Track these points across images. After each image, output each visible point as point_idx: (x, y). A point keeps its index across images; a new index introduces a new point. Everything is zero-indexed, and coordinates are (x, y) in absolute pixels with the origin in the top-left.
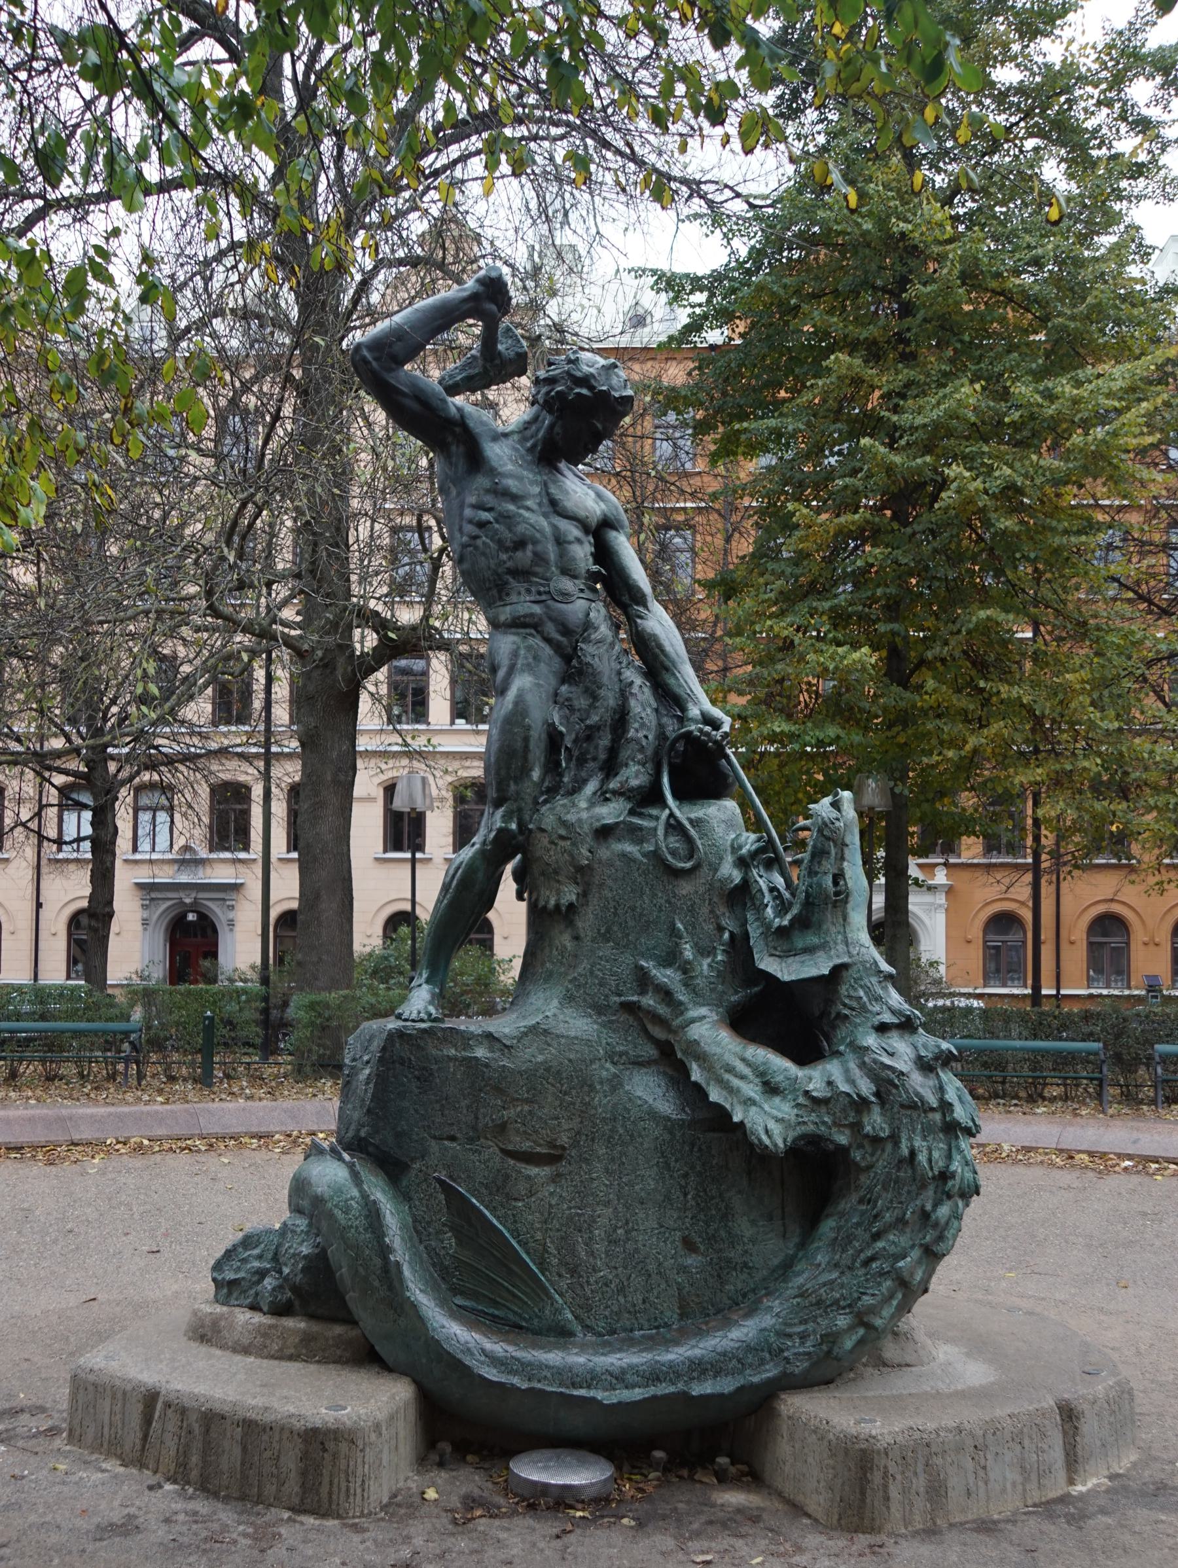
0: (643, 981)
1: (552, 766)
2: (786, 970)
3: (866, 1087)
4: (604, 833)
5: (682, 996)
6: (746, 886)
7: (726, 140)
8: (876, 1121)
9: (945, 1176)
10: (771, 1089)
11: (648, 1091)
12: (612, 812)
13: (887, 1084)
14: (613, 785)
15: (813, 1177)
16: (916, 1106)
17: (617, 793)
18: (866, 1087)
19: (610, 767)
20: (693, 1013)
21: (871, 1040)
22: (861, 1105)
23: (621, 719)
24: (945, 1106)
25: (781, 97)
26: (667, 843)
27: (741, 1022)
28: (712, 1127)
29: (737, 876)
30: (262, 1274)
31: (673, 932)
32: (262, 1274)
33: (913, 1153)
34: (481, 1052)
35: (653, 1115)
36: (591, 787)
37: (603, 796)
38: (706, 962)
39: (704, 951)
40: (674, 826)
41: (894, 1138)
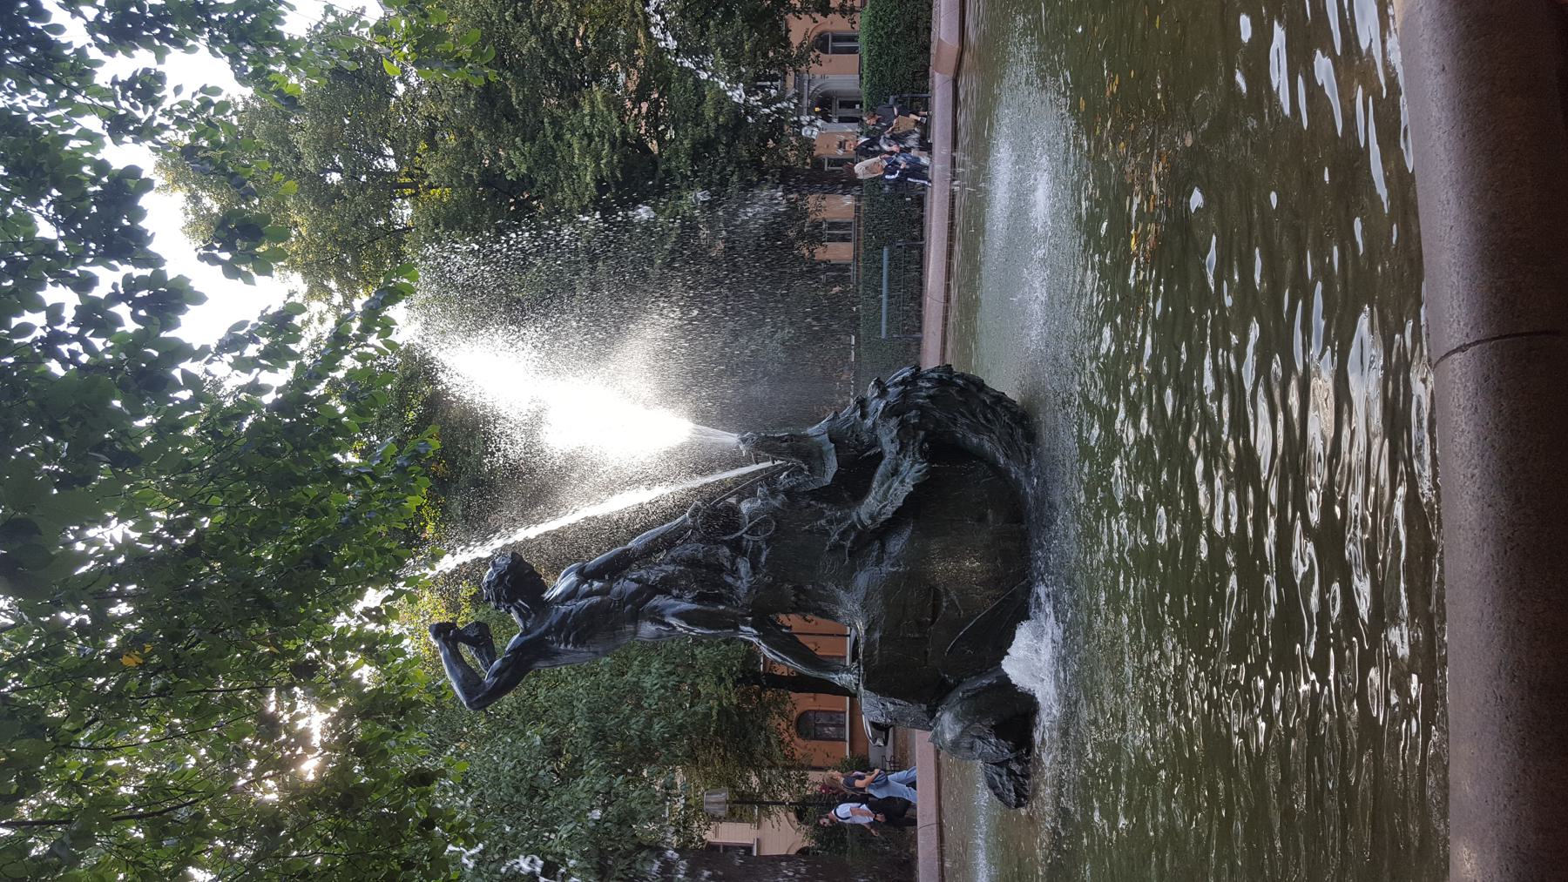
0: (837, 548)
1: (719, 599)
2: (832, 466)
3: (894, 422)
4: (754, 568)
5: (845, 525)
6: (788, 492)
7: (178, 90)
8: (913, 417)
9: (940, 381)
10: (895, 472)
11: (896, 545)
12: (744, 566)
13: (889, 412)
14: (728, 565)
15: (944, 453)
16: (904, 395)
17: (733, 563)
18: (894, 422)
19: (720, 569)
20: (855, 518)
21: (869, 422)
22: (903, 425)
23: (692, 563)
24: (904, 382)
25: (281, 325)
26: (760, 537)
27: (860, 494)
28: (913, 507)
29: (781, 496)
30: (1011, 773)
31: (810, 532)
32: (1011, 773)
33: (929, 397)
34: (877, 635)
35: (911, 540)
36: (730, 580)
37: (734, 572)
38: (827, 513)
39: (821, 514)
40: (753, 531)
41: (920, 407)
